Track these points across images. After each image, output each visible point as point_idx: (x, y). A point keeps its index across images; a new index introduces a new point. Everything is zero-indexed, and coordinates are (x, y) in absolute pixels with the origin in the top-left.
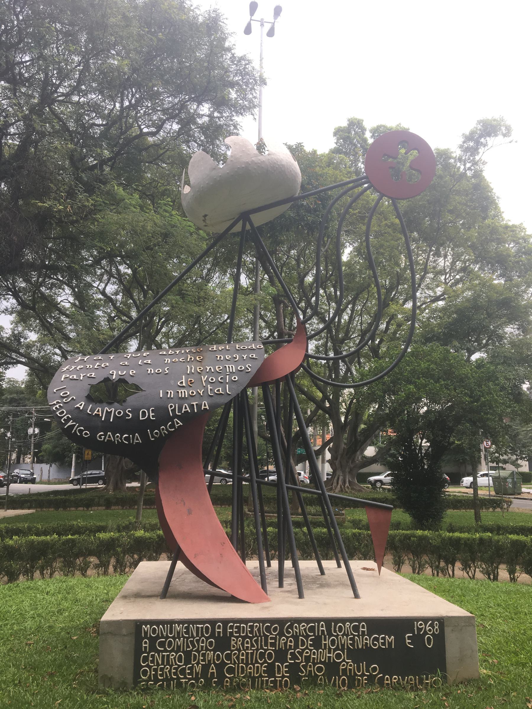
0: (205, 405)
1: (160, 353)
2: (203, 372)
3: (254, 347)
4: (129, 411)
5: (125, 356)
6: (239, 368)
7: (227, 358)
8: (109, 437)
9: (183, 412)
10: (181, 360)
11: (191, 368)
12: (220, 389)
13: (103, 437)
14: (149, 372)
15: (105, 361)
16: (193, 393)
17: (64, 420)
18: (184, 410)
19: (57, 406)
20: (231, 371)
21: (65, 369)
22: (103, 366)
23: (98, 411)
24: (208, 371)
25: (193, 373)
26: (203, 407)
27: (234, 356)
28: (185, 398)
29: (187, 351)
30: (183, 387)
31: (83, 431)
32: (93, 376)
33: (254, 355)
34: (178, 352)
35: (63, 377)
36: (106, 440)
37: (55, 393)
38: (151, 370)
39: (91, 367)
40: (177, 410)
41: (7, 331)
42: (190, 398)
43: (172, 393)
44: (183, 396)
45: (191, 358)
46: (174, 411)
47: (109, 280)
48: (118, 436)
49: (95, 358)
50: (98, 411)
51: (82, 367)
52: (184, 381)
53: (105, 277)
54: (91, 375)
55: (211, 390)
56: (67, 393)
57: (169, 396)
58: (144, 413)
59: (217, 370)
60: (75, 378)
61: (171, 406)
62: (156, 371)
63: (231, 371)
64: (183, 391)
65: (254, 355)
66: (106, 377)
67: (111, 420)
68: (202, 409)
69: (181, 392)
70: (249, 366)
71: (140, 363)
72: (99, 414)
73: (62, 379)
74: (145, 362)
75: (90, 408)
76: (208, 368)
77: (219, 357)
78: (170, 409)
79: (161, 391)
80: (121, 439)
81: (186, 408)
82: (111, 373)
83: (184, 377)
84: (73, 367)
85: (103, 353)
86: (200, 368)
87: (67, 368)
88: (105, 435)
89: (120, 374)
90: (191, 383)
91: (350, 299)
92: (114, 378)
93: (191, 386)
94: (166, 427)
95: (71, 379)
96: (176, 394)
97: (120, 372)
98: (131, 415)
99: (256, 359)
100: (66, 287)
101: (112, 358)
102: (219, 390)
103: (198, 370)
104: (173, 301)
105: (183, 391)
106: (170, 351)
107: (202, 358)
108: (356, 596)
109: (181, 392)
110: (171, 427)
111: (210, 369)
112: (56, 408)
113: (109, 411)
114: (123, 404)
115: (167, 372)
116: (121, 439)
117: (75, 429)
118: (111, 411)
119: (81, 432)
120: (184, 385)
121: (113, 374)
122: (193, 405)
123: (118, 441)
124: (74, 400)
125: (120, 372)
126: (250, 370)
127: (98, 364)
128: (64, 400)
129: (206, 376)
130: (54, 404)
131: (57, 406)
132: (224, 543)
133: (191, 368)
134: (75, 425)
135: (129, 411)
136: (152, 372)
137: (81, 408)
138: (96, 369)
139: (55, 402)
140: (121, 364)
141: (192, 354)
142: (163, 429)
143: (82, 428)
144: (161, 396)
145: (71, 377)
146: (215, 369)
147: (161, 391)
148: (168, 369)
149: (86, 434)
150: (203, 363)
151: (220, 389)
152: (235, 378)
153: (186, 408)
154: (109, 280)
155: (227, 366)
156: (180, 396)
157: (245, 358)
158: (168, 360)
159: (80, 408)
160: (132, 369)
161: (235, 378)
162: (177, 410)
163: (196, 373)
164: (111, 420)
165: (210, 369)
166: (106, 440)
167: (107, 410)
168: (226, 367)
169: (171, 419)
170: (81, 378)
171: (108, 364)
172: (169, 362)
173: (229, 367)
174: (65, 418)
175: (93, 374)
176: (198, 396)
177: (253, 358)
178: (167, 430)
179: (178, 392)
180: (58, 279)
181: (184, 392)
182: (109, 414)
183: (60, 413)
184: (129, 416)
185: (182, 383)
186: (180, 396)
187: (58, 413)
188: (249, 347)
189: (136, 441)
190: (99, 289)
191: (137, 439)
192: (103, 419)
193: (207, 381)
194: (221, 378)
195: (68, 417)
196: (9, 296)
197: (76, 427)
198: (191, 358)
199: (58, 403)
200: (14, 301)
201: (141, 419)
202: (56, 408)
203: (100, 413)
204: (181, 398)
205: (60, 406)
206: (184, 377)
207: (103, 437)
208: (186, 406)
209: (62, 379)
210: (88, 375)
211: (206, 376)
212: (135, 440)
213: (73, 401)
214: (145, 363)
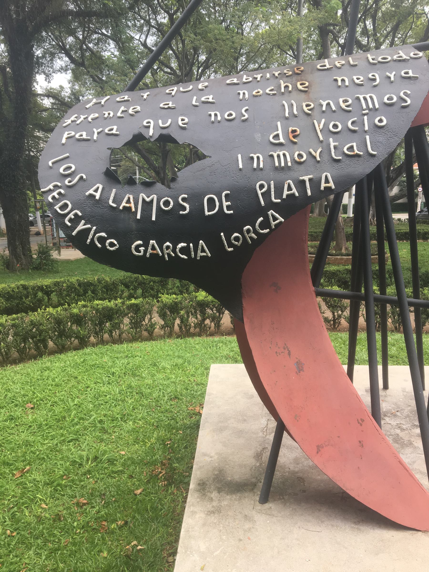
0: (327, 181)
1: (228, 82)
2: (316, 113)
3: (405, 57)
4: (184, 200)
5: (167, 91)
6: (386, 100)
7: (357, 81)
8: (153, 248)
9: (284, 196)
10: (267, 91)
11: (291, 106)
12: (354, 144)
13: (142, 249)
14: (213, 119)
15: (135, 103)
16: (300, 156)
17: (70, 220)
18: (286, 193)
19: (55, 194)
20: (371, 106)
21: (69, 121)
22: (131, 111)
23: (128, 201)
24: (324, 108)
25: (296, 116)
26: (323, 185)
27: (370, 76)
28: (286, 168)
29: (276, 74)
30: (281, 144)
31: (105, 239)
32: (114, 132)
33: (410, 72)
34: (259, 77)
35: (66, 135)
36: (148, 255)
37: (51, 168)
38: (216, 115)
39: (111, 115)
40: (273, 193)
41: (66, 90)
42: (296, 166)
43: (261, 159)
44: (283, 164)
45: (287, 87)
46: (267, 194)
47: (149, 31)
48: (168, 247)
49: (118, 99)
50: (128, 201)
51: (97, 115)
52: (280, 132)
53: (145, 29)
54: (112, 130)
55: (335, 147)
56: (70, 168)
57: (255, 165)
58: (211, 201)
59: (343, 106)
60: (84, 137)
61: (262, 187)
62: (226, 117)
63: (371, 106)
64: (281, 154)
65: (410, 72)
66: (136, 132)
67: (154, 218)
68: (322, 188)
69: (279, 156)
70: (405, 94)
71: (194, 103)
72: (130, 208)
73: (64, 141)
74: (203, 99)
75: (113, 195)
76: (324, 104)
77: (339, 79)
78: (259, 192)
79: (240, 156)
80: (174, 251)
81: (290, 189)
82: (145, 123)
83: (279, 124)
84: (82, 117)
85: (132, 88)
86: (183, 120)
87: (73, 118)
88: (146, 245)
89: (161, 125)
90: (294, 137)
91: (389, 29)
92: (151, 134)
93: (295, 143)
94: (254, 227)
95: (79, 140)
96: (269, 160)
97: (160, 122)
98: (187, 206)
99: (416, 78)
100: (111, 42)
101: (145, 97)
102: (352, 147)
103: (306, 109)
104: (216, 31)
105: (281, 154)
106: (245, 77)
107: (307, 84)
108: (210, 157)
109: (279, 156)
110: (263, 226)
111: (328, 104)
112: (54, 198)
113: (148, 200)
114: (172, 185)
115: (247, 116)
116: (174, 251)
117: (90, 237)
118: (152, 201)
119: (102, 240)
120: (282, 140)
121: (149, 127)
122: (304, 182)
123: (169, 255)
124: (85, 180)
125: (160, 122)
126: (409, 102)
127: (123, 108)
128: (66, 182)
129: (323, 121)
130: (50, 191)
131: (55, 194)
132: (363, 420)
133: (291, 106)
134: (89, 230)
135: (184, 200)
136: (219, 118)
137: (98, 196)
138: (120, 117)
139: (51, 187)
140: (161, 105)
141: (286, 79)
142: (248, 231)
143: (103, 234)
144: (241, 166)
145: (77, 136)
146: (337, 104)
147: (240, 156)
148: (246, 110)
149: (112, 245)
150: (311, 95)
151: (354, 144)
152: (381, 121)
153: (290, 189)
154: (149, 31)
155: (361, 97)
156: (277, 164)
157: (392, 79)
158: (245, 93)
159: (94, 196)
160: (181, 115)
161: (381, 121)
162: (273, 193)
163: (302, 115)
164: (154, 218)
165: (328, 104)
166: (148, 255)
167: (144, 200)
168: (358, 99)
169: (263, 212)
170: (95, 138)
171: (139, 108)
172: (247, 96)
173: (365, 99)
174: (71, 216)
175: (115, 128)
176: (312, 161)
177: (409, 78)
178: (255, 232)
179: (272, 156)
180: (103, 34)
181: (284, 155)
182: (147, 205)
183: (61, 208)
184: (184, 209)
185: (277, 137)
186: (277, 164)
187: (57, 208)
188: (395, 57)
189: (200, 254)
190: (140, 41)
191: (203, 251)
192: (139, 217)
193: (325, 130)
194: (353, 123)
195: (76, 215)
196: (62, 55)
197: (92, 232)
198: (287, 87)
199: (56, 187)
200: (67, 59)
201: (207, 213)
202: (54, 198)
203: (132, 205)
204: (280, 169)
205: (60, 194)
206: (279, 124)
207: (142, 249)
208: (289, 185)
209: (64, 141)
210: (106, 131)
211: (323, 121)
212: (199, 251)
213: (81, 183)
214: (204, 102)
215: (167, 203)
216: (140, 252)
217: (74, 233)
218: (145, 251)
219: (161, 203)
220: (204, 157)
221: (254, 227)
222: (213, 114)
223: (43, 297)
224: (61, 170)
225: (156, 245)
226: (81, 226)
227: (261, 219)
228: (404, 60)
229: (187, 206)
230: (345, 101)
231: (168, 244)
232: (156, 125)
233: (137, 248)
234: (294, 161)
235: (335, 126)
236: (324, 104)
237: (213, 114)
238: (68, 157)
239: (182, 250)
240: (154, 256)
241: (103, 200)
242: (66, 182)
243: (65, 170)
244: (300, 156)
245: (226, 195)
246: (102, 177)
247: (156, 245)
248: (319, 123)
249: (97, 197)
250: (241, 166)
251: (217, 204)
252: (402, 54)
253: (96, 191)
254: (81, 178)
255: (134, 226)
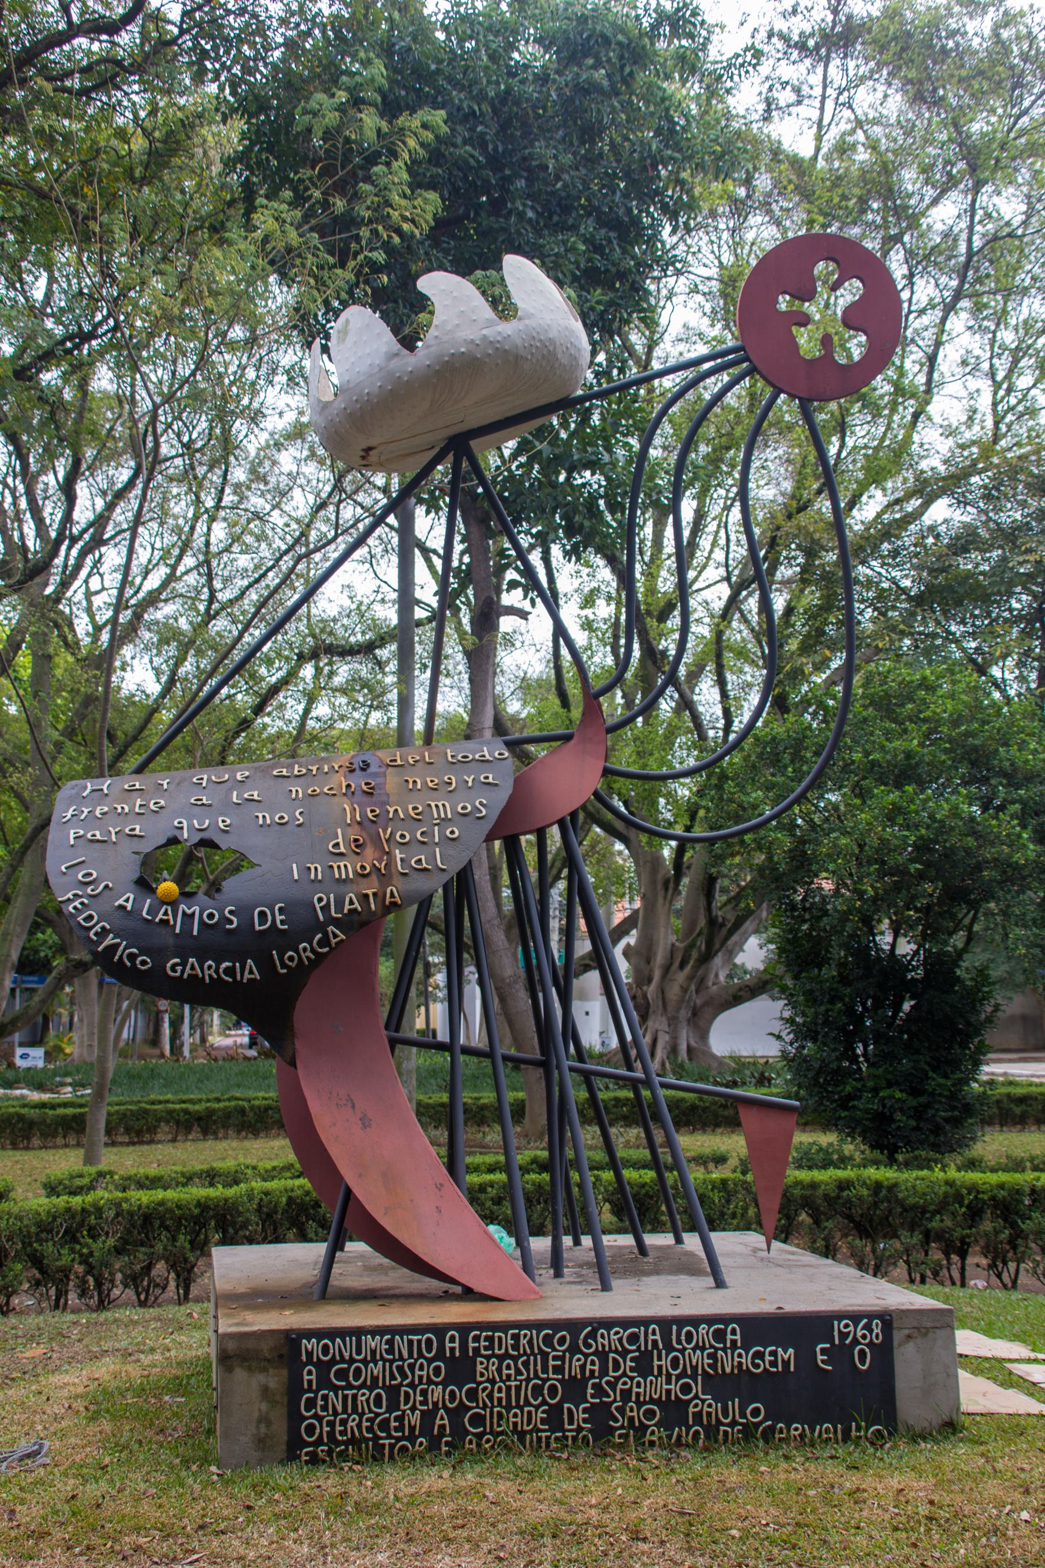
6: (459, 810)
7: (431, 785)
8: (193, 968)
13: (179, 968)
14: (261, 822)
16: (363, 867)
17: (96, 934)
18: (347, 907)
19: (77, 904)
30: (342, 854)
32: (137, 832)
36: (185, 976)
40: (333, 907)
43: (319, 869)
46: (326, 909)
52: (340, 840)
55: (402, 860)
57: (313, 876)
58: (262, 914)
60: (99, 837)
61: (320, 900)
64: (342, 864)
67: (195, 933)
70: (481, 803)
71: (235, 800)
74: (246, 796)
76: (391, 810)
78: (317, 906)
80: (217, 971)
82: (176, 823)
83: (339, 831)
84: (86, 811)
88: (184, 964)
94: (311, 944)
95: (92, 841)
96: (328, 871)
98: (235, 920)
103: (370, 815)
109: (339, 867)
110: (321, 944)
112: (75, 908)
114: (216, 896)
117: (119, 953)
118: (193, 914)
119: (132, 957)
120: (342, 850)
122: (366, 896)
123: (210, 976)
128: (89, 891)
131: (77, 904)
134: (118, 945)
135: (231, 912)
137: (129, 906)
139: (70, 895)
143: (135, 950)
144: (296, 877)
145: (89, 836)
146: (406, 811)
153: (351, 903)
155: (433, 804)
158: (297, 790)
160: (221, 815)
161: (452, 832)
162: (333, 907)
163: (367, 823)
164: (195, 933)
166: (185, 976)
167: (184, 912)
173: (437, 806)
174: (98, 928)
175: (138, 827)
179: (331, 867)
182: (188, 917)
183: (86, 919)
184: (231, 922)
185: (337, 845)
187: (80, 919)
192: (178, 931)
194: (423, 833)
195: (103, 928)
199: (75, 895)
201: (257, 928)
205: (82, 903)
206: (339, 831)
209: (72, 842)
210: (127, 831)
215: (211, 916)
216: (175, 971)
217: (100, 949)
218: (183, 972)
219: (205, 915)
220: (253, 865)
221: (311, 944)
222: (260, 815)
223: (673, 631)
224: (80, 877)
225: (196, 965)
226: (109, 940)
227: (319, 936)
228: (488, 761)
229: (235, 920)
230: (415, 808)
231: (210, 962)
232: (191, 827)
233: (173, 968)
234: (355, 872)
235: (403, 836)
236: (391, 810)
237: (260, 815)
238: (83, 862)
239: (227, 971)
240: (193, 977)
241: (135, 912)
242: (89, 891)
243: (84, 876)
244: (363, 867)
245: (280, 909)
246: (132, 886)
247: (196, 965)
248: (385, 833)
249: (129, 908)
250: (296, 877)
251: (270, 918)
252: (486, 753)
253: (127, 900)
254: (107, 886)
255: (171, 941)
